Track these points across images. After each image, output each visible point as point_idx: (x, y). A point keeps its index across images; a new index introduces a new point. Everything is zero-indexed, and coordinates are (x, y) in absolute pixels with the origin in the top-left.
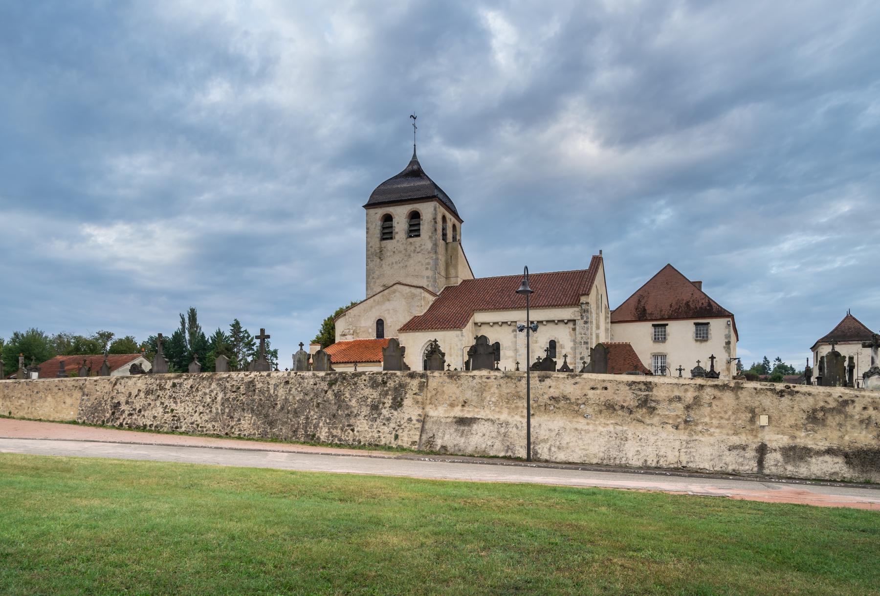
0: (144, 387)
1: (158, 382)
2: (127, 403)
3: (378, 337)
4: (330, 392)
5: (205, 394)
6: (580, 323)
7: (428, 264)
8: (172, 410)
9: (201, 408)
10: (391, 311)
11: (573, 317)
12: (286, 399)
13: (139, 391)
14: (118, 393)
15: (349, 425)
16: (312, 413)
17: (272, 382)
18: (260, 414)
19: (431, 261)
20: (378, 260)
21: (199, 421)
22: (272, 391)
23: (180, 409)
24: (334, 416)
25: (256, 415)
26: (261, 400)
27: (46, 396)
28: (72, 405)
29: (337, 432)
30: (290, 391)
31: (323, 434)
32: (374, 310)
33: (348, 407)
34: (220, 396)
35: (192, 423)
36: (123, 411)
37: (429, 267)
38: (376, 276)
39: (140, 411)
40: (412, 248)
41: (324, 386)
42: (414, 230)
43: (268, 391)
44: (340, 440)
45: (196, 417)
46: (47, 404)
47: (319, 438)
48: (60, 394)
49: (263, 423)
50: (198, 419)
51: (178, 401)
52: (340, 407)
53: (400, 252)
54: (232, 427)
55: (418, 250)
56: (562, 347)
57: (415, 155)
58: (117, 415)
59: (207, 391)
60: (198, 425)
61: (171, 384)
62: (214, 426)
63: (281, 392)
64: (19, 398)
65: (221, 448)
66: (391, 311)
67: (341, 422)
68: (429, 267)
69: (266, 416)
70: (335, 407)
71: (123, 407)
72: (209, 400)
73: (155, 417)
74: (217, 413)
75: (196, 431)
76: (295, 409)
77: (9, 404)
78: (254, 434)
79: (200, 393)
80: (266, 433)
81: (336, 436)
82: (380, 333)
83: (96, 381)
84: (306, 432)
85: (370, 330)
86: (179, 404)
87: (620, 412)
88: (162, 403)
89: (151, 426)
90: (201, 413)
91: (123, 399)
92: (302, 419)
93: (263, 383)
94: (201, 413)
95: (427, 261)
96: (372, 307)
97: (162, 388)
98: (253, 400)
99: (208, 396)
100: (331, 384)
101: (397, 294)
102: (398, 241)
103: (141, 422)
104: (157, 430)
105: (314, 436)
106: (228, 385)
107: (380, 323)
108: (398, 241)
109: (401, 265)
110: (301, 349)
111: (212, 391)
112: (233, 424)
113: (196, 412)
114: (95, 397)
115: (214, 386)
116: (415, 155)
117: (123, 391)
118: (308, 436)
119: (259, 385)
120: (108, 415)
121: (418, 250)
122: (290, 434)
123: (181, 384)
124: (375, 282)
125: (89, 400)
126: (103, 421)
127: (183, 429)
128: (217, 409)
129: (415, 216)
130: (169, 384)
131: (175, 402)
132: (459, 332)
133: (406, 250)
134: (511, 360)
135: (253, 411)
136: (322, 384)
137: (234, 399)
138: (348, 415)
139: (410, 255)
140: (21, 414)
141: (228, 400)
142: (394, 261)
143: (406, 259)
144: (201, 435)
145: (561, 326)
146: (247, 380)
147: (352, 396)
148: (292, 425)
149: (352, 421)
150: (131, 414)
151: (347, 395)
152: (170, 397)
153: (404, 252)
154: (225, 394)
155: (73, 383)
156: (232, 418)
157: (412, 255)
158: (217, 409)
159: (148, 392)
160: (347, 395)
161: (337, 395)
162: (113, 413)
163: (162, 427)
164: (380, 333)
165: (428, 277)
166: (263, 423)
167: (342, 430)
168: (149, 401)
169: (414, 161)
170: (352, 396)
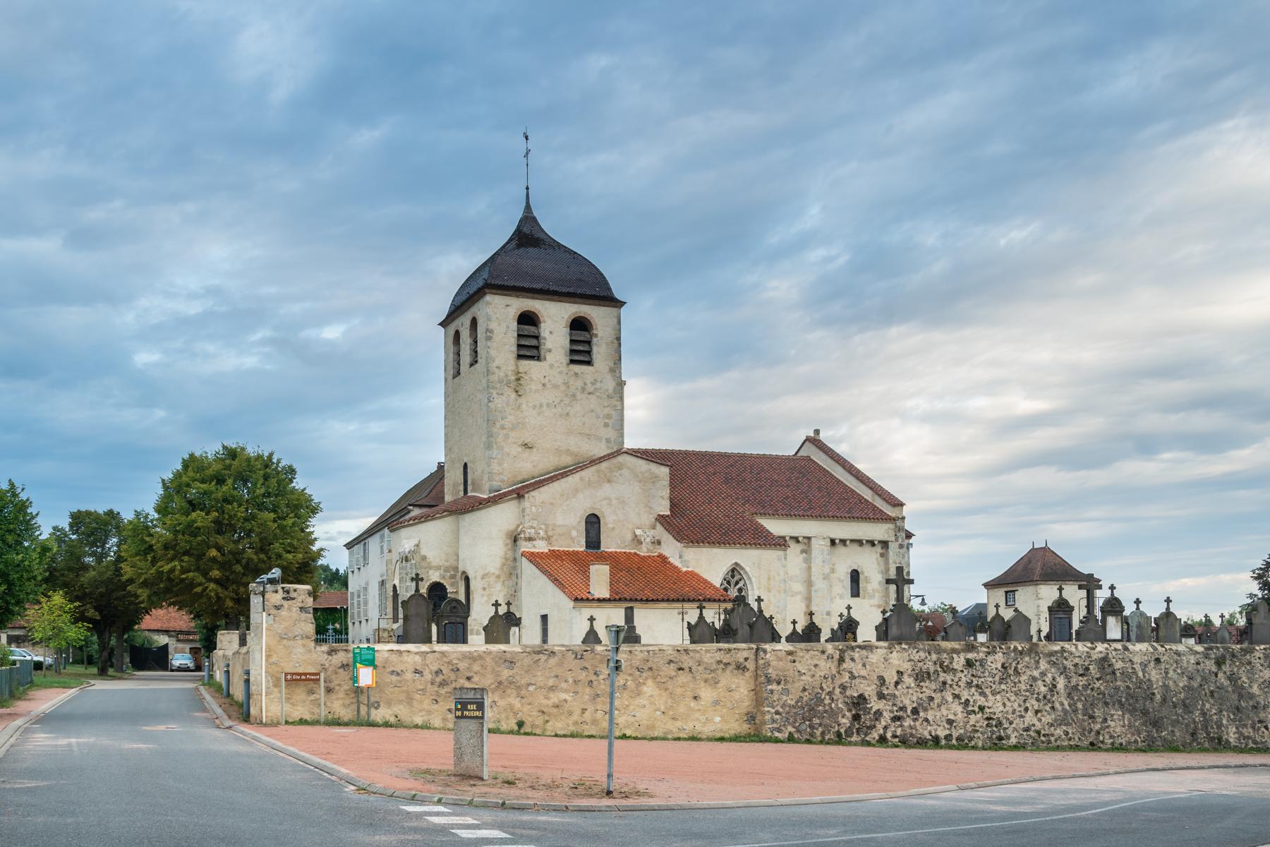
0: (906, 666)
1: (934, 657)
2: (881, 696)
3: (588, 545)
4: (1220, 675)
5: (1034, 679)
6: (893, 547)
7: (608, 416)
8: (982, 709)
9: (1033, 703)
10: (614, 502)
11: (885, 538)
12: (1164, 685)
13: (900, 673)
14: (853, 677)
15: (1260, 722)
16: (1208, 706)
17: (1137, 659)
18: (1135, 710)
19: (613, 413)
20: (513, 395)
21: (1038, 726)
22: (1140, 674)
23: (996, 705)
24: (1238, 709)
25: (1130, 712)
26: (1128, 687)
27: (639, 685)
28: (716, 703)
29: (1248, 731)
30: (1167, 673)
31: (1231, 735)
32: (580, 496)
33: (1252, 696)
34: (1061, 683)
35: (1027, 729)
36: (878, 714)
37: (610, 422)
38: (508, 425)
39: (915, 711)
40: (579, 384)
41: (1210, 665)
42: (529, 347)
43: (1135, 673)
44: (1255, 742)
45: (1030, 718)
46: (642, 701)
47: (1227, 741)
48: (683, 678)
49: (1144, 724)
50: (1035, 721)
51: (988, 691)
52: (1241, 696)
53: (556, 386)
54: (1098, 733)
55: (590, 388)
56: (867, 580)
57: (528, 207)
58: (866, 719)
59: (1036, 673)
60: (1038, 732)
61: (962, 661)
62: (1067, 733)
63: (1154, 675)
64: (552, 689)
65: (1247, 766)
66: (614, 502)
67: (1248, 717)
68: (610, 422)
69: (1145, 713)
70: (1235, 697)
71: (875, 705)
72: (1043, 689)
73: (950, 722)
74: (1064, 710)
75: (1037, 742)
76: (1183, 701)
77: (517, 703)
78: (1136, 741)
79: (1024, 678)
80: (1153, 740)
81: (1249, 738)
82: (593, 541)
83: (790, 653)
84: (1208, 733)
85: (574, 533)
86: (990, 697)
87: (973, 690)
88: (957, 697)
89: (949, 737)
90: (1037, 712)
91: (869, 690)
92: (1197, 715)
93: (1123, 660)
94: (1037, 712)
95: (607, 411)
96: (577, 491)
97: (947, 669)
98: (1117, 689)
99: (1040, 683)
100: (1219, 662)
101: (625, 472)
102: (551, 366)
103: (925, 732)
104: (963, 743)
105: (1220, 739)
106: (1068, 664)
107: (593, 523)
108: (551, 366)
109: (559, 410)
110: (1138, 608)
111: (1043, 674)
112: (1098, 726)
113: (1026, 710)
114: (800, 685)
115: (1043, 665)
116: (528, 207)
117: (863, 673)
118: (1212, 739)
119: (1119, 665)
120: (845, 722)
121: (590, 388)
122: (1188, 739)
123: (982, 663)
124: (507, 437)
125: (786, 692)
126: (839, 735)
127: (1013, 741)
128: (1062, 704)
129: (528, 319)
130: (959, 661)
131: (983, 694)
132: (781, 553)
133: (566, 384)
134: (799, 597)
135: (1122, 705)
136: (1208, 663)
137: (1085, 687)
138: (1255, 707)
139: (574, 396)
140: (559, 726)
141: (1075, 687)
142: (545, 402)
143: (567, 401)
144: (1048, 749)
145: (868, 548)
146: (1096, 656)
147: (1251, 681)
148: (1187, 725)
149: (1262, 715)
150: (896, 719)
151: (1244, 679)
152: (969, 684)
153: (563, 388)
154: (1068, 678)
155: (719, 656)
156: (1092, 717)
157: (579, 396)
158: (1062, 704)
159: (921, 676)
160: (1244, 679)
161: (1232, 678)
162: (856, 718)
163: (971, 739)
164: (593, 541)
165: (608, 441)
166: (1144, 724)
167: (1253, 728)
168: (928, 693)
169: (528, 218)
170: (1251, 681)
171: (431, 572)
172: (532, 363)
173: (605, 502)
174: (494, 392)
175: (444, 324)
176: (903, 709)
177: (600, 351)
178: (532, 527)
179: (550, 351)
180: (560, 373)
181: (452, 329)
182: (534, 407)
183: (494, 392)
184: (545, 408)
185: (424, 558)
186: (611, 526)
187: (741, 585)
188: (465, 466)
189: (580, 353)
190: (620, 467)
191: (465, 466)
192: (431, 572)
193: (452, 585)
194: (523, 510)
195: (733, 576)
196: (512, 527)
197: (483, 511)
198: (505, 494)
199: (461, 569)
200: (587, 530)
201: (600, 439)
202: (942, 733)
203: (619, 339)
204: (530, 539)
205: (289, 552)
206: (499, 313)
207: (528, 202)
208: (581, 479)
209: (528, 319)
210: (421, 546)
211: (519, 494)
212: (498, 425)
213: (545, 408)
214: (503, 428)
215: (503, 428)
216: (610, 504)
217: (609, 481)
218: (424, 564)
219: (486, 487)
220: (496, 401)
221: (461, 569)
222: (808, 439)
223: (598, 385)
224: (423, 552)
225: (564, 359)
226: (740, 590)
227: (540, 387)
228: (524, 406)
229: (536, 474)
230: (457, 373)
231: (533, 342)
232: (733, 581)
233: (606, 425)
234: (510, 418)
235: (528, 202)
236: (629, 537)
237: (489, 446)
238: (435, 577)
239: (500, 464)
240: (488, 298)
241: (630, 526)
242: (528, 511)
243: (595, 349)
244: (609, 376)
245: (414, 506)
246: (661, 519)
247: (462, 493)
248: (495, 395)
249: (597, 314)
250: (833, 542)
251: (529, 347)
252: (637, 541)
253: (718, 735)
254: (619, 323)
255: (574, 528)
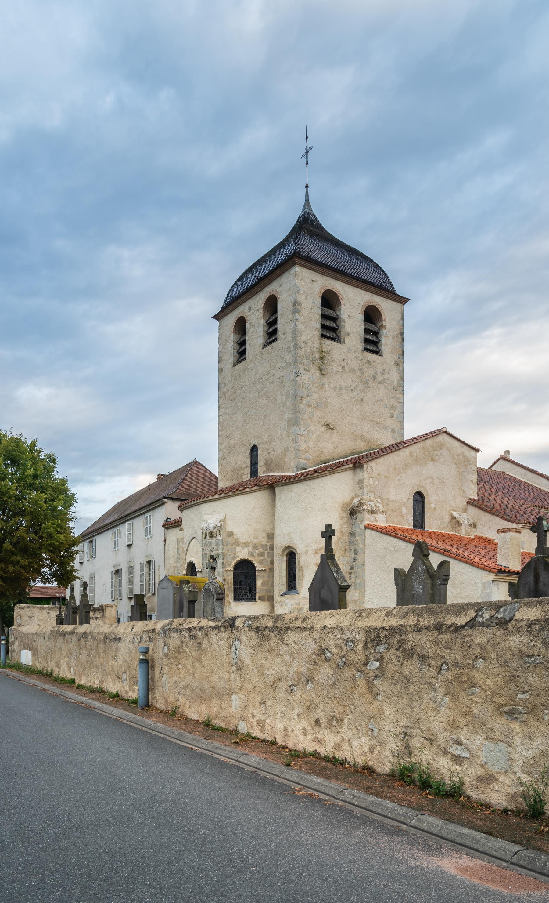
10: (436, 481)
20: (318, 373)
38: (313, 403)
40: (371, 372)
42: (331, 329)
53: (352, 371)
55: (380, 378)
57: (307, 202)
66: (436, 481)
101: (444, 452)
124: (312, 415)
129: (329, 301)
139: (367, 383)
143: (362, 386)
153: (359, 374)
157: (371, 384)
171: (238, 549)
172: (334, 343)
173: (429, 481)
174: (302, 367)
175: (218, 317)
177: (387, 341)
178: (370, 500)
180: (356, 358)
182: (335, 389)
183: (302, 367)
184: (343, 391)
185: (231, 534)
186: (433, 506)
188: (254, 449)
189: (372, 343)
190: (441, 446)
191: (254, 449)
192: (238, 549)
193: (261, 563)
194: (361, 482)
196: (347, 500)
197: (317, 481)
198: (342, 464)
199: (281, 542)
200: (414, 508)
201: (387, 428)
203: (402, 334)
204: (372, 512)
205: (58, 532)
206: (302, 288)
207: (307, 200)
208: (411, 454)
209: (329, 301)
210: (227, 521)
211: (357, 464)
212: (305, 401)
213: (343, 391)
214: (309, 405)
215: (309, 405)
216: (432, 484)
217: (432, 460)
218: (230, 540)
219: (293, 464)
220: (304, 377)
221: (281, 542)
222: (502, 458)
223: (386, 376)
224: (230, 527)
225: (360, 346)
227: (340, 369)
228: (326, 386)
229: (336, 456)
230: (241, 354)
231: (333, 325)
234: (315, 396)
235: (307, 200)
236: (447, 518)
237: (294, 422)
238: (243, 554)
239: (306, 442)
240: (297, 269)
241: (448, 508)
242: (366, 483)
243: (384, 340)
244: (394, 369)
245: (168, 498)
246: (471, 502)
248: (302, 371)
249: (385, 305)
251: (331, 329)
252: (456, 522)
254: (402, 319)
255: (404, 504)
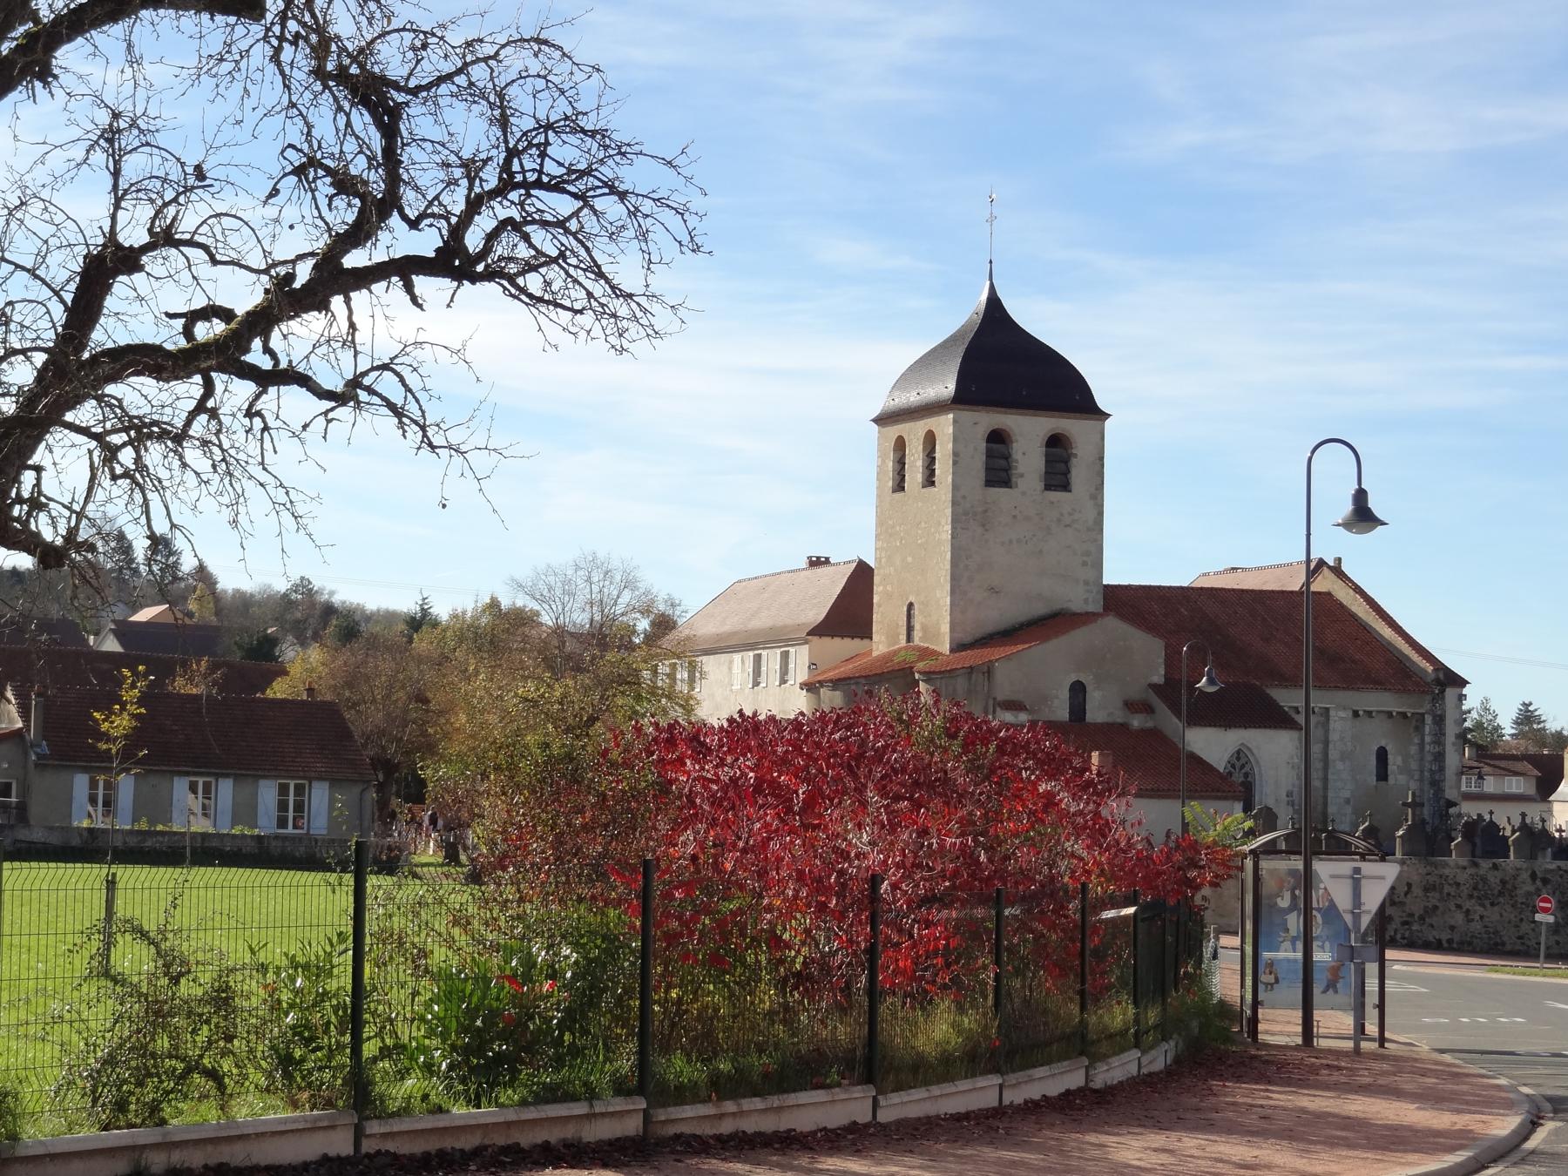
39: (1422, 918)
57: (992, 287)
73: (1452, 928)
88: (1459, 907)
89: (1450, 941)
102: (1024, 493)
116: (992, 287)
129: (998, 438)
131: (1483, 906)
176: (1411, 915)
177: (1078, 474)
179: (1022, 476)
181: (894, 431)
187: (1247, 769)
195: (1238, 759)
202: (1445, 937)
209: (998, 438)
226: (1246, 775)
232: (1238, 765)
233: (1085, 564)
247: (903, 638)
250: (1356, 714)
253: (979, 633)
